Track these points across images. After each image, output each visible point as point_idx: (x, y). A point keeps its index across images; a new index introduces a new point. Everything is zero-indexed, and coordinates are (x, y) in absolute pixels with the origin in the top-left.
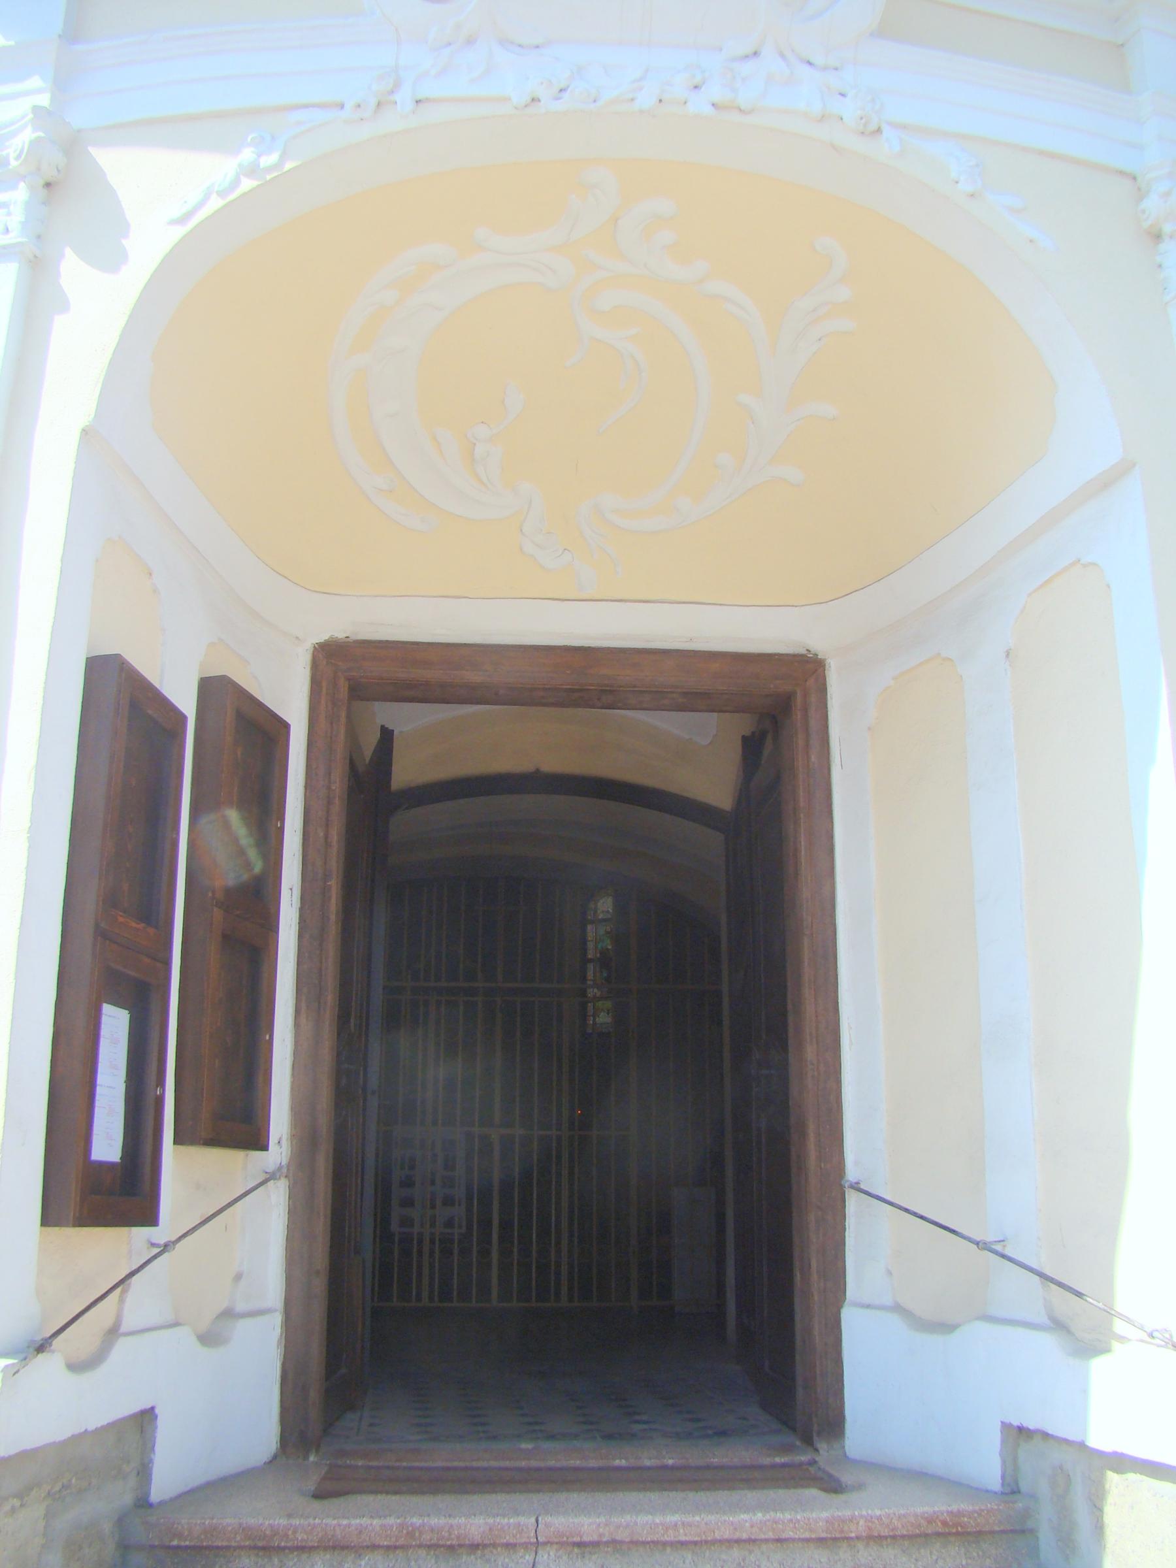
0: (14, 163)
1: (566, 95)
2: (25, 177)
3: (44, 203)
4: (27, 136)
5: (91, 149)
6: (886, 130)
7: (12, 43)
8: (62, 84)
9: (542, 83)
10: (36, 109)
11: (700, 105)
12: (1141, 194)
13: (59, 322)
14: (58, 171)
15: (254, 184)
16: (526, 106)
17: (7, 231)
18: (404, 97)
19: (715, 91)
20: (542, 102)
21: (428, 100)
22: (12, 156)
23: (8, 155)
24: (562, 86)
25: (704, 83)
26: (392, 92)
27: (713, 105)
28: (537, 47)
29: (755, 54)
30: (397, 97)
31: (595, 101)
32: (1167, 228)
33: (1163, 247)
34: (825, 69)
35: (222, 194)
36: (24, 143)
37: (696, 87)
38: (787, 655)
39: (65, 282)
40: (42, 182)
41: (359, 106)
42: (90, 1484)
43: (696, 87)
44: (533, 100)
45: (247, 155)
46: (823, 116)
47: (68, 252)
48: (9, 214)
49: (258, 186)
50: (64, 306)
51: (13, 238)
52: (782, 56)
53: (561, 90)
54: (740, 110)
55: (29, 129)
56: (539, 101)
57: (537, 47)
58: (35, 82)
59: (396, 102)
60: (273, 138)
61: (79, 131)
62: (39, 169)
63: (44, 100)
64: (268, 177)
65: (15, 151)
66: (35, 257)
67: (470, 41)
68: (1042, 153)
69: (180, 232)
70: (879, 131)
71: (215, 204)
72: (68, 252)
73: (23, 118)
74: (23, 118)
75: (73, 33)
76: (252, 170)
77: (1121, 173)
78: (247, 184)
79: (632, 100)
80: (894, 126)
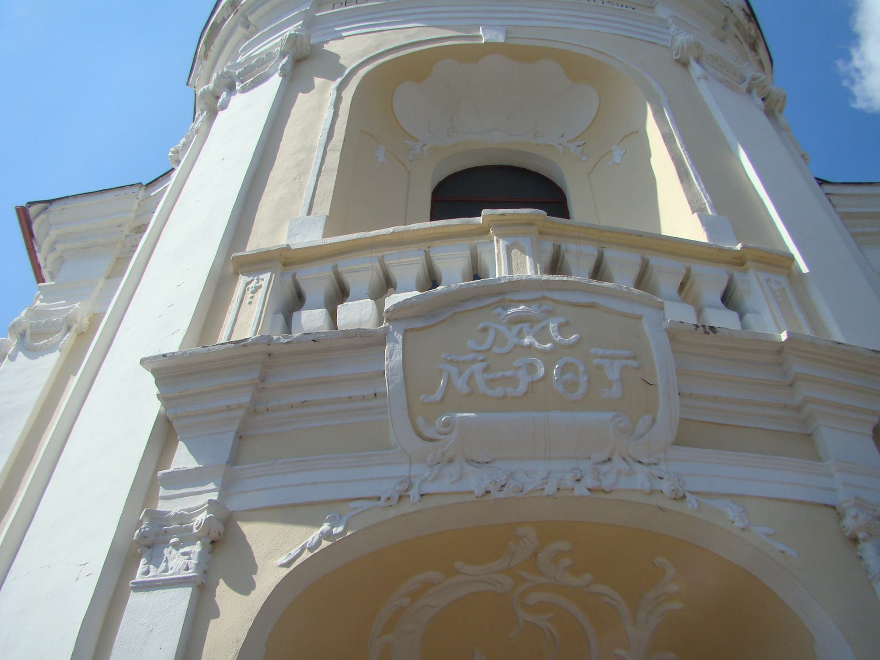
0: (195, 531)
1: (505, 489)
2: (201, 538)
3: (210, 553)
4: (203, 516)
5: (239, 523)
6: (688, 495)
7: (201, 466)
8: (225, 489)
9: (491, 483)
10: (210, 501)
11: (581, 490)
12: (840, 516)
13: (213, 623)
14: (220, 534)
15: (330, 543)
16: (483, 496)
17: (187, 569)
18: (414, 493)
19: (589, 482)
20: (492, 493)
21: (427, 494)
22: (195, 527)
23: (193, 525)
24: (503, 484)
25: (582, 478)
26: (407, 490)
27: (588, 489)
28: (488, 463)
29: (610, 459)
30: (410, 493)
31: (521, 491)
32: (861, 535)
33: (860, 546)
34: (649, 464)
35: (311, 549)
36: (202, 520)
37: (578, 480)
38: (785, 242)
39: (218, 600)
40: (210, 541)
41: (389, 498)
42: (619, 164)
43: (578, 480)
44: (487, 492)
45: (325, 527)
46: (652, 491)
47: (221, 581)
48: (189, 559)
49: (332, 544)
50: (216, 614)
51: (190, 573)
52: (624, 459)
53: (502, 486)
54: (604, 491)
55: (205, 513)
56: (490, 492)
57: (488, 463)
58: (212, 486)
59: (409, 496)
60: (341, 517)
61: (232, 512)
62: (209, 534)
63: (214, 496)
64: (337, 540)
65: (196, 525)
66: (202, 583)
67: (450, 461)
68: (778, 500)
69: (285, 571)
70: (684, 497)
71: (307, 555)
72: (221, 581)
73: (203, 505)
74: (203, 505)
75: (234, 460)
76: (327, 535)
77: (826, 505)
78: (325, 544)
79: (543, 489)
80: (693, 493)
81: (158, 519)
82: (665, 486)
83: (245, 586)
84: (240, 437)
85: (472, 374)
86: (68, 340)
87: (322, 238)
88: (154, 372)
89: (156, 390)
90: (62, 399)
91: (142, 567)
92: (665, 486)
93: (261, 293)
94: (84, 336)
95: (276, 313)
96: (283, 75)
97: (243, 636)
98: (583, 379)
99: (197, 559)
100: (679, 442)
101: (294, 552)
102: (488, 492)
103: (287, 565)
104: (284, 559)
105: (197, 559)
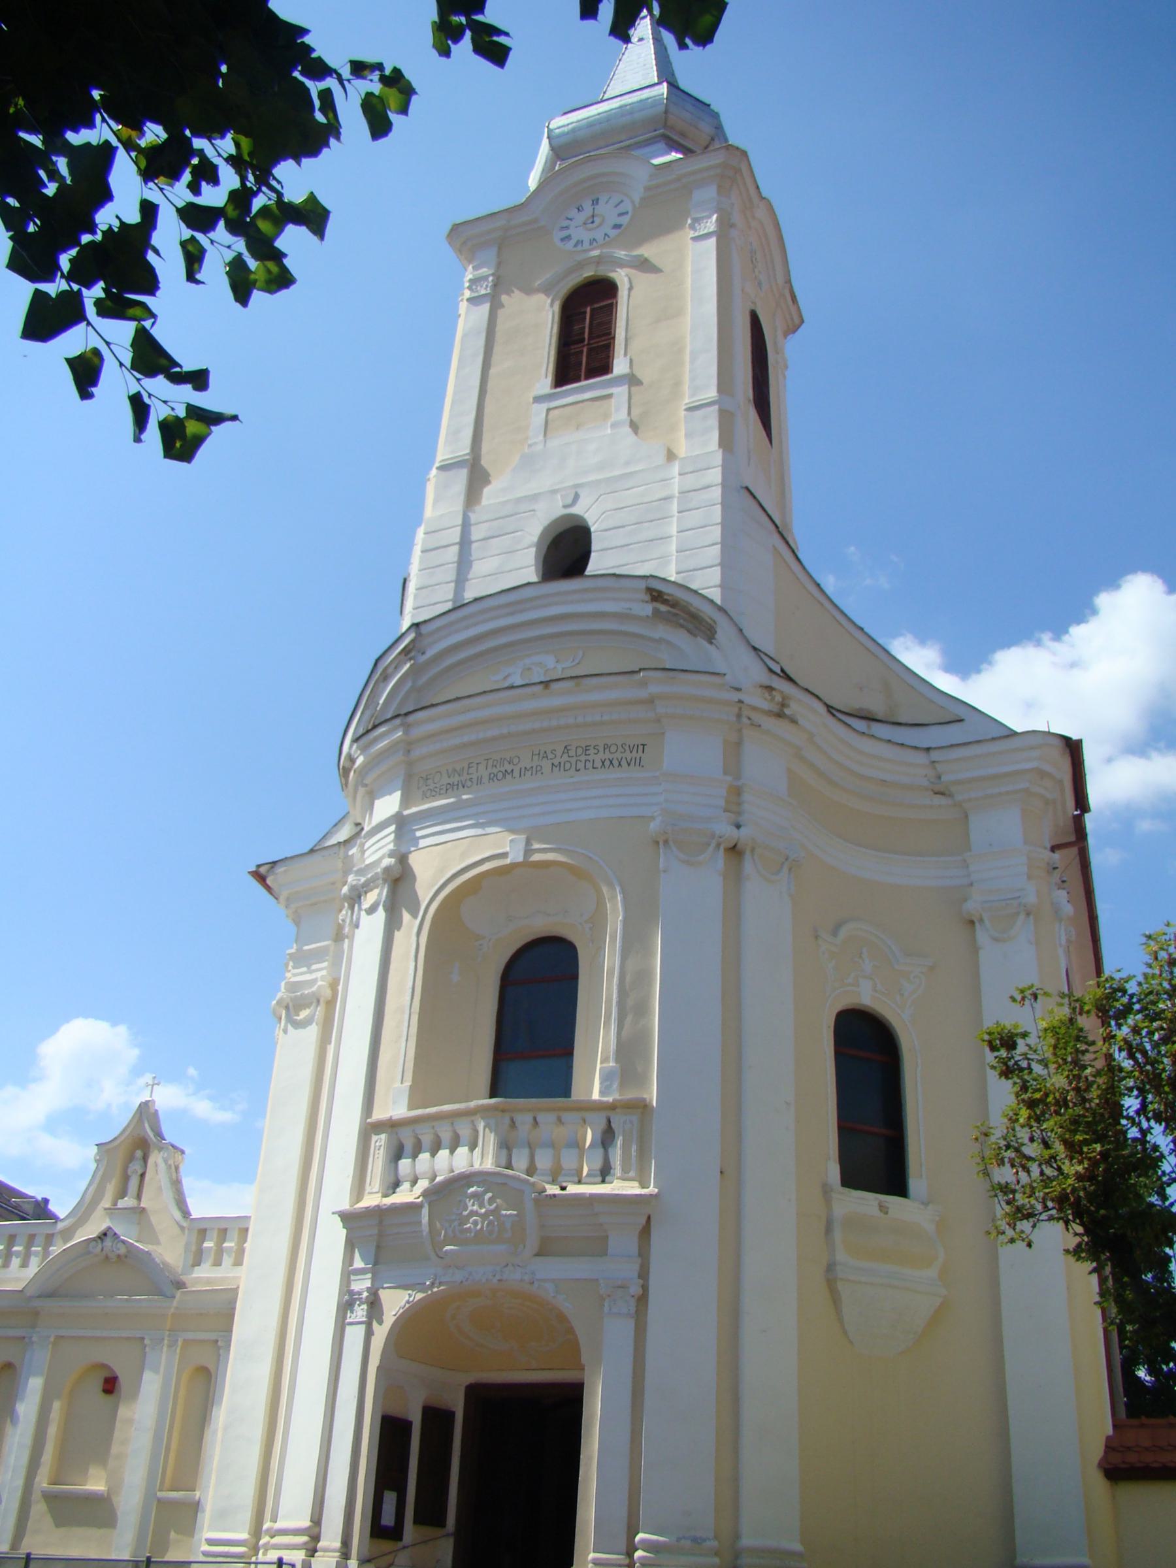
8: (373, 1280)
69: (396, 1317)
70: (533, 1283)
71: (401, 1311)
78: (407, 1306)
81: (351, 1293)
82: (526, 1278)
83: (380, 1322)
84: (378, 1247)
85: (454, 1227)
86: (320, 1012)
87: (408, 1110)
88: (339, 1216)
89: (341, 1224)
90: (283, 1374)
91: (349, 1315)
92: (526, 1278)
93: (382, 1148)
94: (331, 1004)
95: (391, 1162)
96: (386, 910)
97: (382, 1345)
98: (496, 1229)
99: (990, 663)
100: (537, 1255)
101: (397, 1309)
102: (462, 1282)
103: (395, 1315)
104: (394, 1313)
105: (990, 663)
